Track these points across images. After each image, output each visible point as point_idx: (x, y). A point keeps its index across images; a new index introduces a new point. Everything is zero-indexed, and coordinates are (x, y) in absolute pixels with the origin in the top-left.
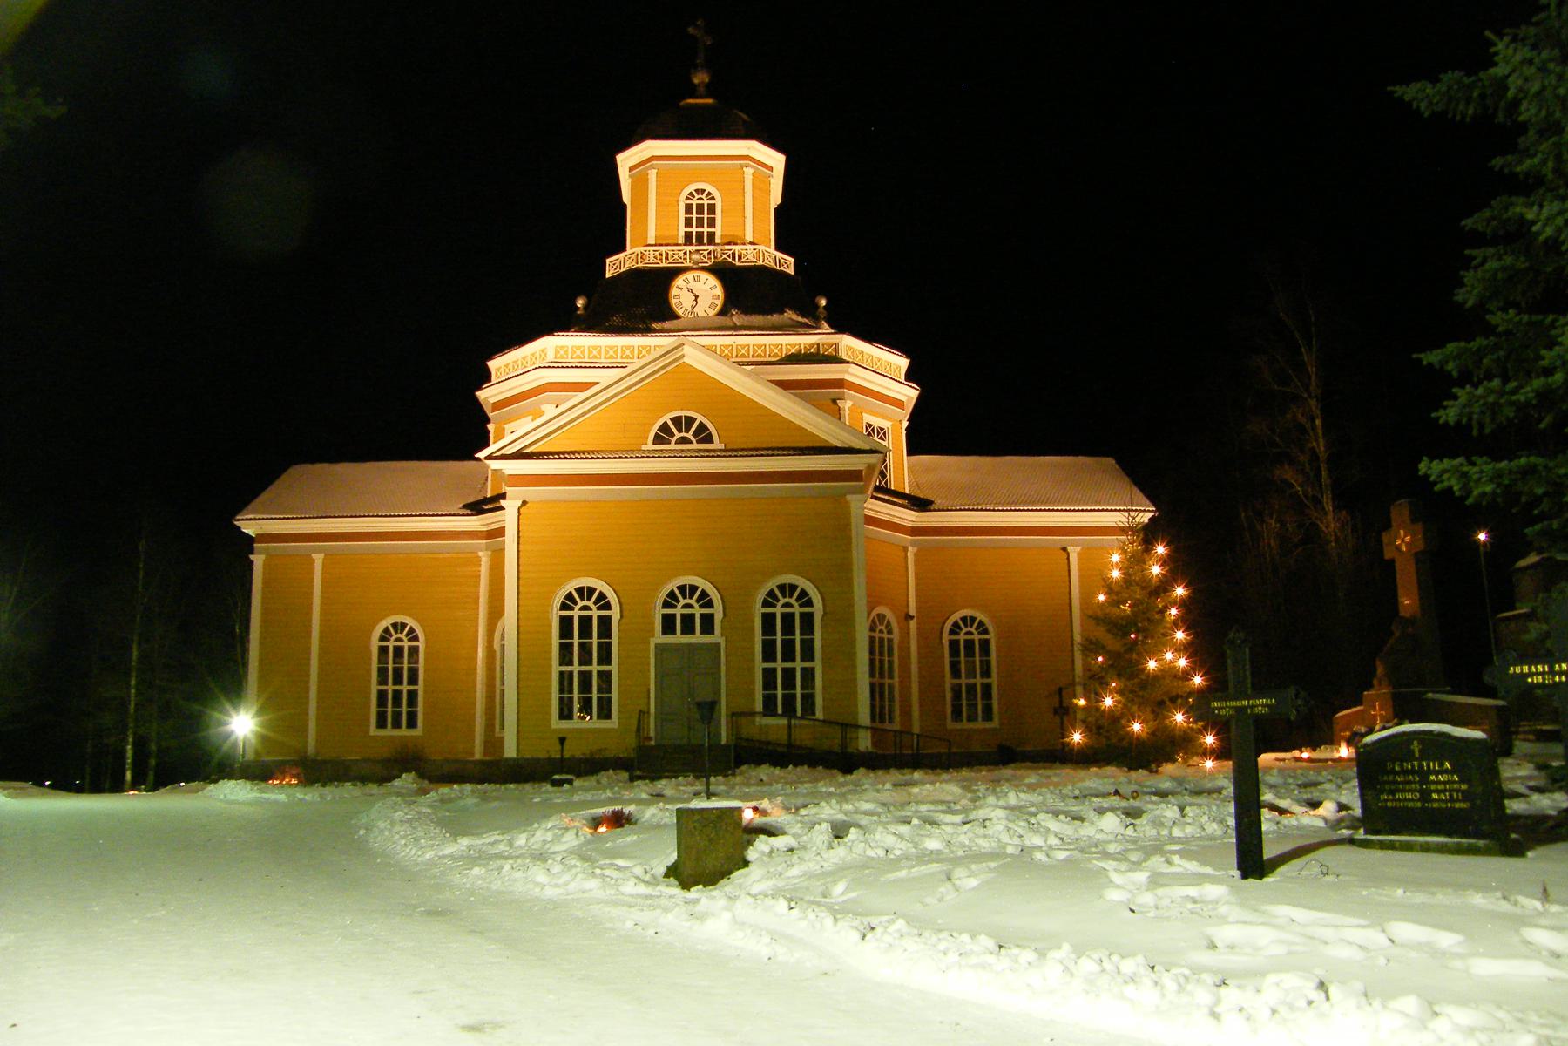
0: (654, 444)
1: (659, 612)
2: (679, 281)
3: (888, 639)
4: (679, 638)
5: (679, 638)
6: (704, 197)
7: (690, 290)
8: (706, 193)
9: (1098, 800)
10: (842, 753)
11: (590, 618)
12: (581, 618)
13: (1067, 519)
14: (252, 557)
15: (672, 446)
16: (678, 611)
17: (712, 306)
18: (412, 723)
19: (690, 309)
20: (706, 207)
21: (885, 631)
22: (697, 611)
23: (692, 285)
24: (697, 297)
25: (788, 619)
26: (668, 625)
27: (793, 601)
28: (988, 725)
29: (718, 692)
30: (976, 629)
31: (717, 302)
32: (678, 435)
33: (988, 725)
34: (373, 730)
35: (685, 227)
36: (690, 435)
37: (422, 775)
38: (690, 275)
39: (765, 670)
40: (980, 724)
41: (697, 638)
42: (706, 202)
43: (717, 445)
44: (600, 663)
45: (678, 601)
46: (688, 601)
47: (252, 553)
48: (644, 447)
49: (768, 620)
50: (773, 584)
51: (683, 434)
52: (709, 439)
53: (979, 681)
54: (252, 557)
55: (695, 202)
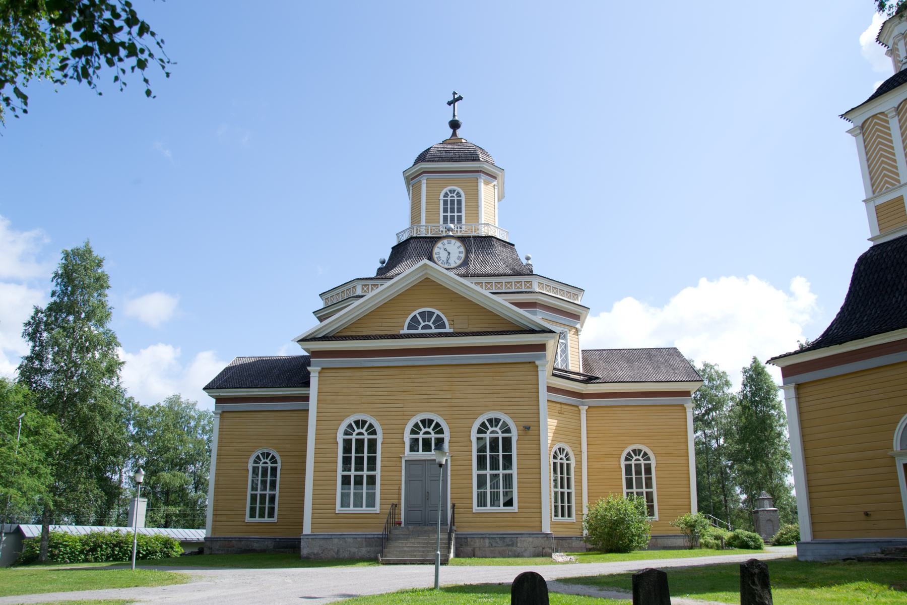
0: (408, 329)
2: (440, 244)
3: (560, 463)
4: (421, 455)
5: (421, 455)
6: (454, 195)
7: (445, 250)
8: (456, 193)
9: (531, 539)
10: (550, 556)
13: (608, 388)
14: (309, 368)
15: (420, 331)
16: (421, 436)
17: (459, 258)
18: (271, 515)
19: (445, 261)
20: (452, 214)
21: (565, 459)
22: (433, 436)
23: (447, 246)
24: (449, 253)
26: (414, 447)
27: (363, 431)
28: (271, 520)
29: (400, 499)
30: (642, 457)
31: (461, 255)
32: (423, 324)
33: (271, 520)
34: (248, 519)
35: (461, 215)
36: (430, 324)
38: (445, 241)
40: (266, 519)
43: (448, 330)
44: (492, 469)
45: (421, 430)
47: (310, 366)
48: (402, 332)
50: (436, 419)
52: (443, 326)
53: (268, 492)
54: (309, 368)
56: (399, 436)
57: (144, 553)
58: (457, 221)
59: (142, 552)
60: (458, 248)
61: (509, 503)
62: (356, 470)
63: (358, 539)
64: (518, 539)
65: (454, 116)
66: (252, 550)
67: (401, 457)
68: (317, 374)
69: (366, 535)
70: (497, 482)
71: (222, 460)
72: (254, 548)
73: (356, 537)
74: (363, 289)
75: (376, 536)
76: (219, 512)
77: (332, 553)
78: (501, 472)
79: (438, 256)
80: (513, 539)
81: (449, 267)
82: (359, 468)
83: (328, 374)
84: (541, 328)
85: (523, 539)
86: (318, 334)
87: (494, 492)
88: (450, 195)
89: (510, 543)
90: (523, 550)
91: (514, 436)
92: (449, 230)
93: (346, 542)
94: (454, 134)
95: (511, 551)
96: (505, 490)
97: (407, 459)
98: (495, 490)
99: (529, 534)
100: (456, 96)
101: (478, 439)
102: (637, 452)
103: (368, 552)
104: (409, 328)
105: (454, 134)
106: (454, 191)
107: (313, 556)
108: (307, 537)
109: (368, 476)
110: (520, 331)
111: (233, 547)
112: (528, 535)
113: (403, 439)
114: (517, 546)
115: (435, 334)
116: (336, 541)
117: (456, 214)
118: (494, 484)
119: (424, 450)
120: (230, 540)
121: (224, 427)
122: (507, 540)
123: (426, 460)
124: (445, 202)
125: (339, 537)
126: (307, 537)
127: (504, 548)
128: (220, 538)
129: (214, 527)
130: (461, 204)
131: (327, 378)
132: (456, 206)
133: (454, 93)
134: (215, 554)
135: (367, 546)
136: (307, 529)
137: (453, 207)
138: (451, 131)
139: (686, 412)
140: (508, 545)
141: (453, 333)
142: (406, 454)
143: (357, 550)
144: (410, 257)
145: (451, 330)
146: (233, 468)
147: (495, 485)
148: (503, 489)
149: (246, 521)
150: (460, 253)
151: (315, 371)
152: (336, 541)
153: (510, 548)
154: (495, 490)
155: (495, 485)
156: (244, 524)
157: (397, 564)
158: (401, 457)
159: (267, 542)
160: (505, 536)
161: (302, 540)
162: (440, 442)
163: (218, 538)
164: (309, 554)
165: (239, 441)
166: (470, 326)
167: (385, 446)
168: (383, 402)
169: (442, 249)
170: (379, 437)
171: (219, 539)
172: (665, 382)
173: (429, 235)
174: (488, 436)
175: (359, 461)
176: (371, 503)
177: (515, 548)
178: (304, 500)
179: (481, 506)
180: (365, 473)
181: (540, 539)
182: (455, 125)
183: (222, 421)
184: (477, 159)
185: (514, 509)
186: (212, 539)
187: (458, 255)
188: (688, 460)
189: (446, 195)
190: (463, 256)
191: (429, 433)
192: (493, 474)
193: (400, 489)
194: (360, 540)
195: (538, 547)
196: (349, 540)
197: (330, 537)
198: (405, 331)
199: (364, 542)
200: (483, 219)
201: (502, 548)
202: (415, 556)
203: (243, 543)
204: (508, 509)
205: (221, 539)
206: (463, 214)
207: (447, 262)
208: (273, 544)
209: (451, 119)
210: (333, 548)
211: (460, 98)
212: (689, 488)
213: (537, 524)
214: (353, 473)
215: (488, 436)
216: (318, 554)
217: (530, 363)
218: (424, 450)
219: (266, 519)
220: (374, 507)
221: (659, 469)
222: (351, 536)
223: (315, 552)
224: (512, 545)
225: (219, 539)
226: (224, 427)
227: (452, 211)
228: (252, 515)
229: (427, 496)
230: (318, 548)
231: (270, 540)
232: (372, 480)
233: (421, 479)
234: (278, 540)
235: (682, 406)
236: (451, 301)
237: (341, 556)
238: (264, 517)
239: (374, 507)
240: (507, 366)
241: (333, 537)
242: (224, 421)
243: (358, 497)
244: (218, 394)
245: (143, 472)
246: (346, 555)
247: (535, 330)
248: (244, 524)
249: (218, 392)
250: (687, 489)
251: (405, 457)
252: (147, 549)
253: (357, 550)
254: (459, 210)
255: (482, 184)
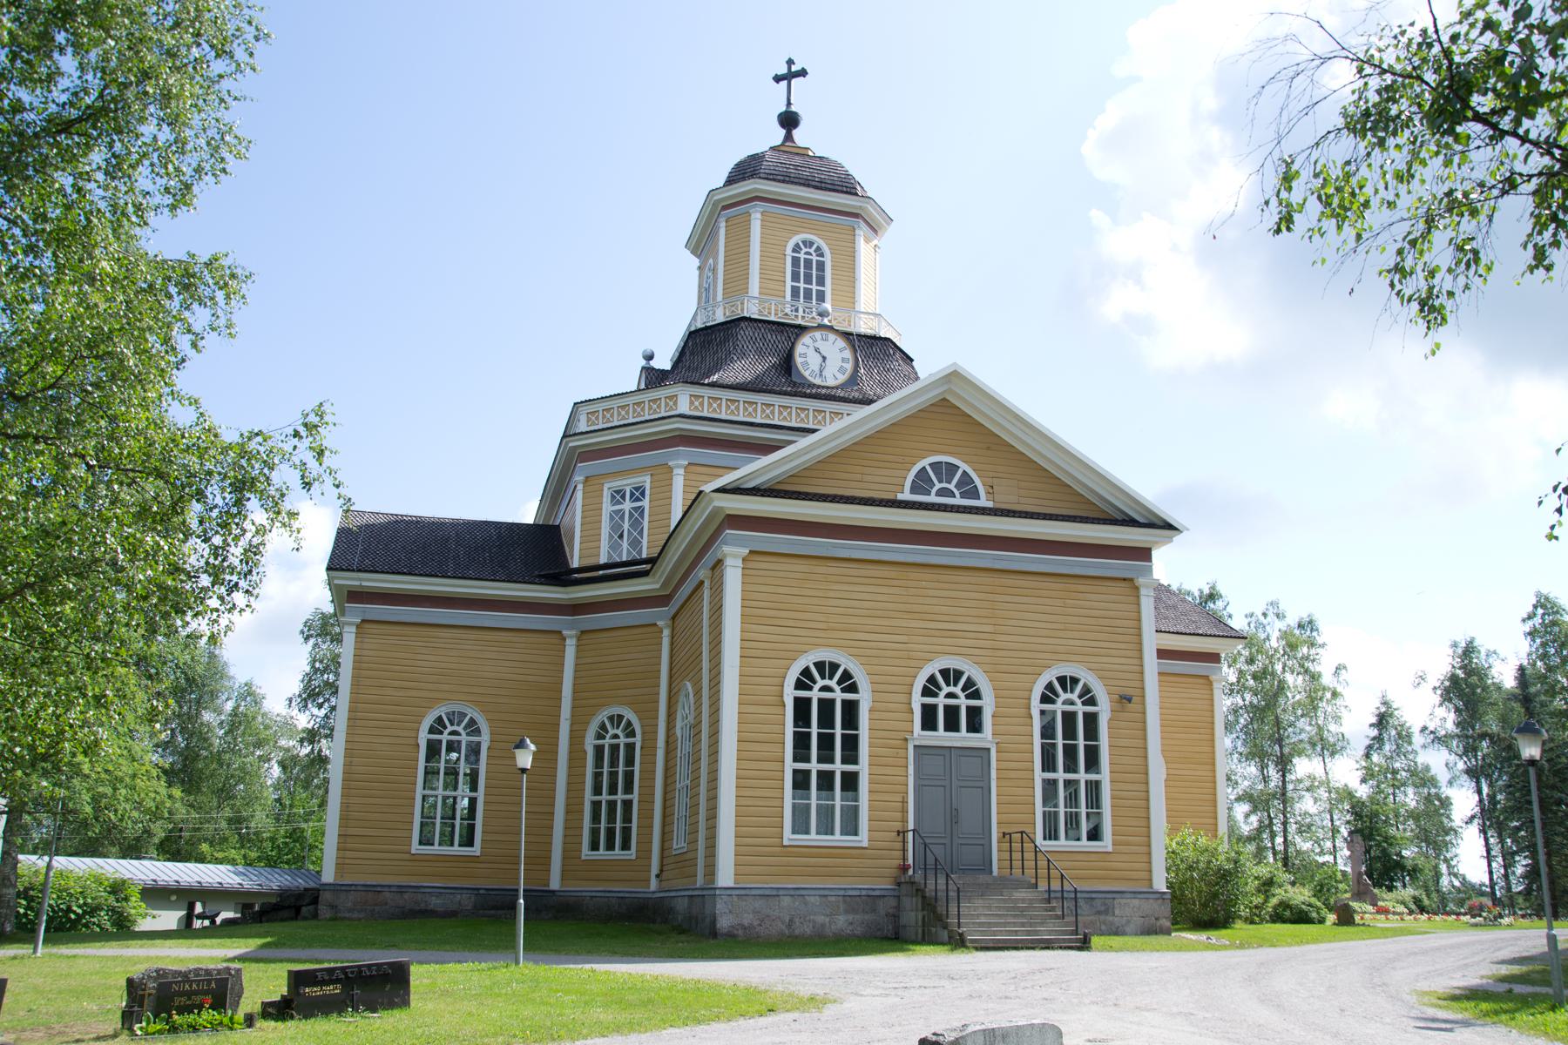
1: (917, 701)
2: (806, 339)
4: (941, 736)
6: (812, 251)
7: (817, 350)
8: (814, 247)
9: (1136, 902)
11: (832, 701)
12: (820, 701)
15: (932, 498)
16: (941, 701)
17: (842, 370)
19: (818, 372)
22: (963, 702)
23: (819, 344)
24: (824, 358)
25: (826, 706)
26: (929, 722)
27: (833, 683)
32: (938, 486)
33: (466, 851)
36: (952, 486)
37: (854, 935)
38: (818, 334)
39: (429, 741)
40: (457, 850)
41: (963, 738)
42: (815, 258)
43: (983, 502)
46: (827, 682)
48: (900, 497)
49: (802, 707)
51: (945, 485)
52: (974, 494)
55: (802, 256)
56: (903, 698)
57: (80, 911)
58: (804, 298)
59: (75, 908)
60: (841, 350)
61: (1094, 835)
62: (844, 761)
63: (829, 898)
64: (1116, 901)
65: (789, 104)
66: (426, 911)
67: (906, 740)
68: (739, 563)
69: (845, 889)
70: (1076, 790)
71: (358, 723)
72: (431, 907)
73: (826, 893)
74: (692, 403)
75: (864, 893)
76: (351, 831)
77: (780, 924)
78: (1082, 776)
79: (804, 360)
80: (1107, 901)
81: (823, 384)
82: (826, 757)
83: (763, 564)
84: (1147, 518)
85: (1124, 901)
86: (745, 482)
87: (1050, 812)
88: (804, 250)
89: (1103, 908)
90: (1124, 922)
91: (1104, 709)
92: (822, 314)
93: (806, 904)
94: (789, 137)
95: (1104, 923)
96: (1068, 810)
97: (917, 744)
98: (1074, 810)
99: (1134, 893)
100: (794, 68)
101: (1043, 712)
102: (951, 676)
103: (851, 923)
104: (914, 490)
105: (789, 137)
106: (811, 244)
107: (740, 932)
108: (729, 892)
109: (820, 773)
110: (1110, 520)
111: (386, 904)
112: (1132, 895)
113: (910, 704)
114: (1114, 915)
115: (959, 506)
116: (786, 901)
117: (814, 287)
118: (1070, 794)
119: (947, 729)
120: (379, 889)
121: (365, 653)
122: (1098, 903)
123: (951, 747)
124: (796, 261)
125: (792, 892)
126: (729, 892)
127: (1092, 918)
128: (356, 885)
129: (340, 861)
130: (823, 271)
131: (761, 573)
132: (802, 270)
133: (790, 62)
134: (344, 918)
135: (847, 912)
136: (726, 876)
137: (809, 272)
138: (783, 132)
139: (1212, 690)
140: (1099, 913)
141: (990, 509)
142: (915, 735)
143: (827, 920)
144: (744, 355)
145: (990, 504)
146: (386, 740)
147: (1072, 799)
148: (1066, 807)
149: (413, 852)
150: (843, 360)
151: (735, 556)
152: (786, 901)
153: (1102, 917)
154: (1074, 810)
155: (1072, 799)
156: (407, 856)
157: (1007, 948)
158: (906, 740)
159: (459, 896)
160: (1094, 895)
161: (718, 899)
162: (975, 715)
163: (351, 885)
164: (733, 927)
165: (397, 683)
166: (1023, 500)
167: (877, 715)
168: (868, 628)
169: (812, 349)
170: (864, 698)
171: (353, 888)
172: (1173, 633)
173: (772, 318)
174: (1059, 707)
175: (826, 742)
176: (851, 827)
177: (1111, 919)
178: (553, 813)
179: (1050, 839)
180: (838, 767)
181: (1151, 901)
182: (789, 121)
183: (359, 640)
184: (853, 191)
185: (1106, 847)
186: (339, 888)
187: (840, 364)
188: (1214, 771)
189: (797, 249)
190: (849, 366)
191: (1072, 703)
192: (1049, 780)
193: (904, 802)
194: (833, 899)
195: (1147, 916)
196: (812, 899)
197: (774, 893)
198: (906, 495)
199: (841, 905)
200: (863, 306)
201: (1090, 918)
202: (1036, 933)
203: (406, 896)
204: (1094, 845)
205: (359, 888)
206: (828, 289)
207: (821, 375)
208: (473, 899)
209: (783, 109)
210: (781, 915)
211: (803, 73)
212: (1216, 818)
213: (1144, 875)
214: (814, 766)
215: (1059, 707)
216: (751, 927)
217: (1124, 579)
218: (947, 729)
219: (457, 850)
220: (856, 834)
221: (1171, 783)
222: (817, 892)
223: (746, 922)
224: (1106, 912)
225: (353, 888)
226: (365, 653)
227: (808, 280)
228: (594, 846)
229: (954, 817)
230: (751, 916)
231: (465, 891)
232: (850, 782)
233: (942, 783)
234: (481, 892)
235: (1207, 677)
236: (988, 448)
237: (797, 932)
238: (598, 849)
239: (856, 834)
240: (1030, 578)
241: (781, 892)
242: (367, 640)
243: (826, 814)
244: (357, 583)
245: (533, 747)
246: (807, 929)
247: (1138, 522)
248: (407, 856)
249: (360, 579)
250: (1211, 821)
251: (913, 739)
252: (85, 904)
253: (827, 920)
254: (821, 281)
255: (862, 239)
